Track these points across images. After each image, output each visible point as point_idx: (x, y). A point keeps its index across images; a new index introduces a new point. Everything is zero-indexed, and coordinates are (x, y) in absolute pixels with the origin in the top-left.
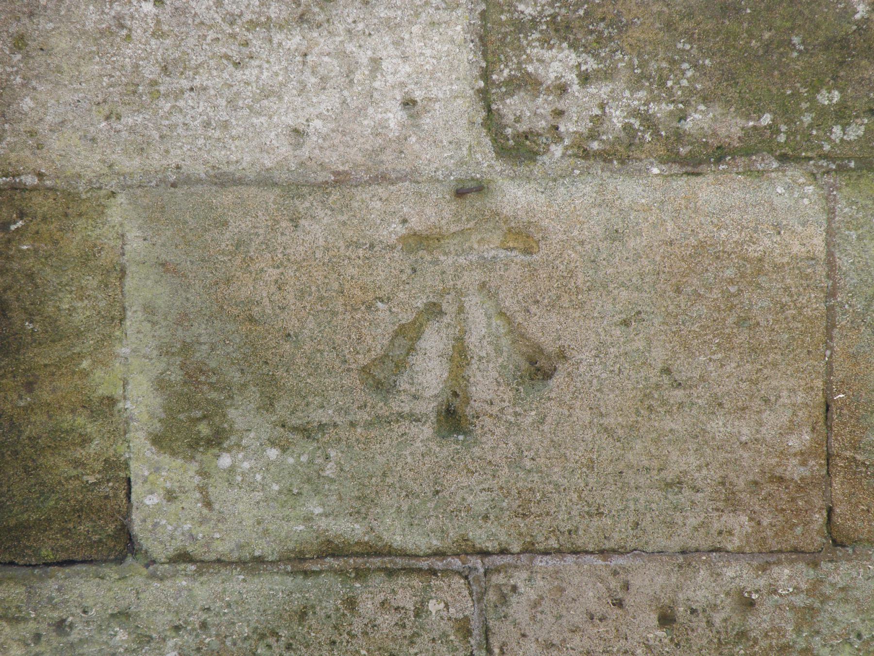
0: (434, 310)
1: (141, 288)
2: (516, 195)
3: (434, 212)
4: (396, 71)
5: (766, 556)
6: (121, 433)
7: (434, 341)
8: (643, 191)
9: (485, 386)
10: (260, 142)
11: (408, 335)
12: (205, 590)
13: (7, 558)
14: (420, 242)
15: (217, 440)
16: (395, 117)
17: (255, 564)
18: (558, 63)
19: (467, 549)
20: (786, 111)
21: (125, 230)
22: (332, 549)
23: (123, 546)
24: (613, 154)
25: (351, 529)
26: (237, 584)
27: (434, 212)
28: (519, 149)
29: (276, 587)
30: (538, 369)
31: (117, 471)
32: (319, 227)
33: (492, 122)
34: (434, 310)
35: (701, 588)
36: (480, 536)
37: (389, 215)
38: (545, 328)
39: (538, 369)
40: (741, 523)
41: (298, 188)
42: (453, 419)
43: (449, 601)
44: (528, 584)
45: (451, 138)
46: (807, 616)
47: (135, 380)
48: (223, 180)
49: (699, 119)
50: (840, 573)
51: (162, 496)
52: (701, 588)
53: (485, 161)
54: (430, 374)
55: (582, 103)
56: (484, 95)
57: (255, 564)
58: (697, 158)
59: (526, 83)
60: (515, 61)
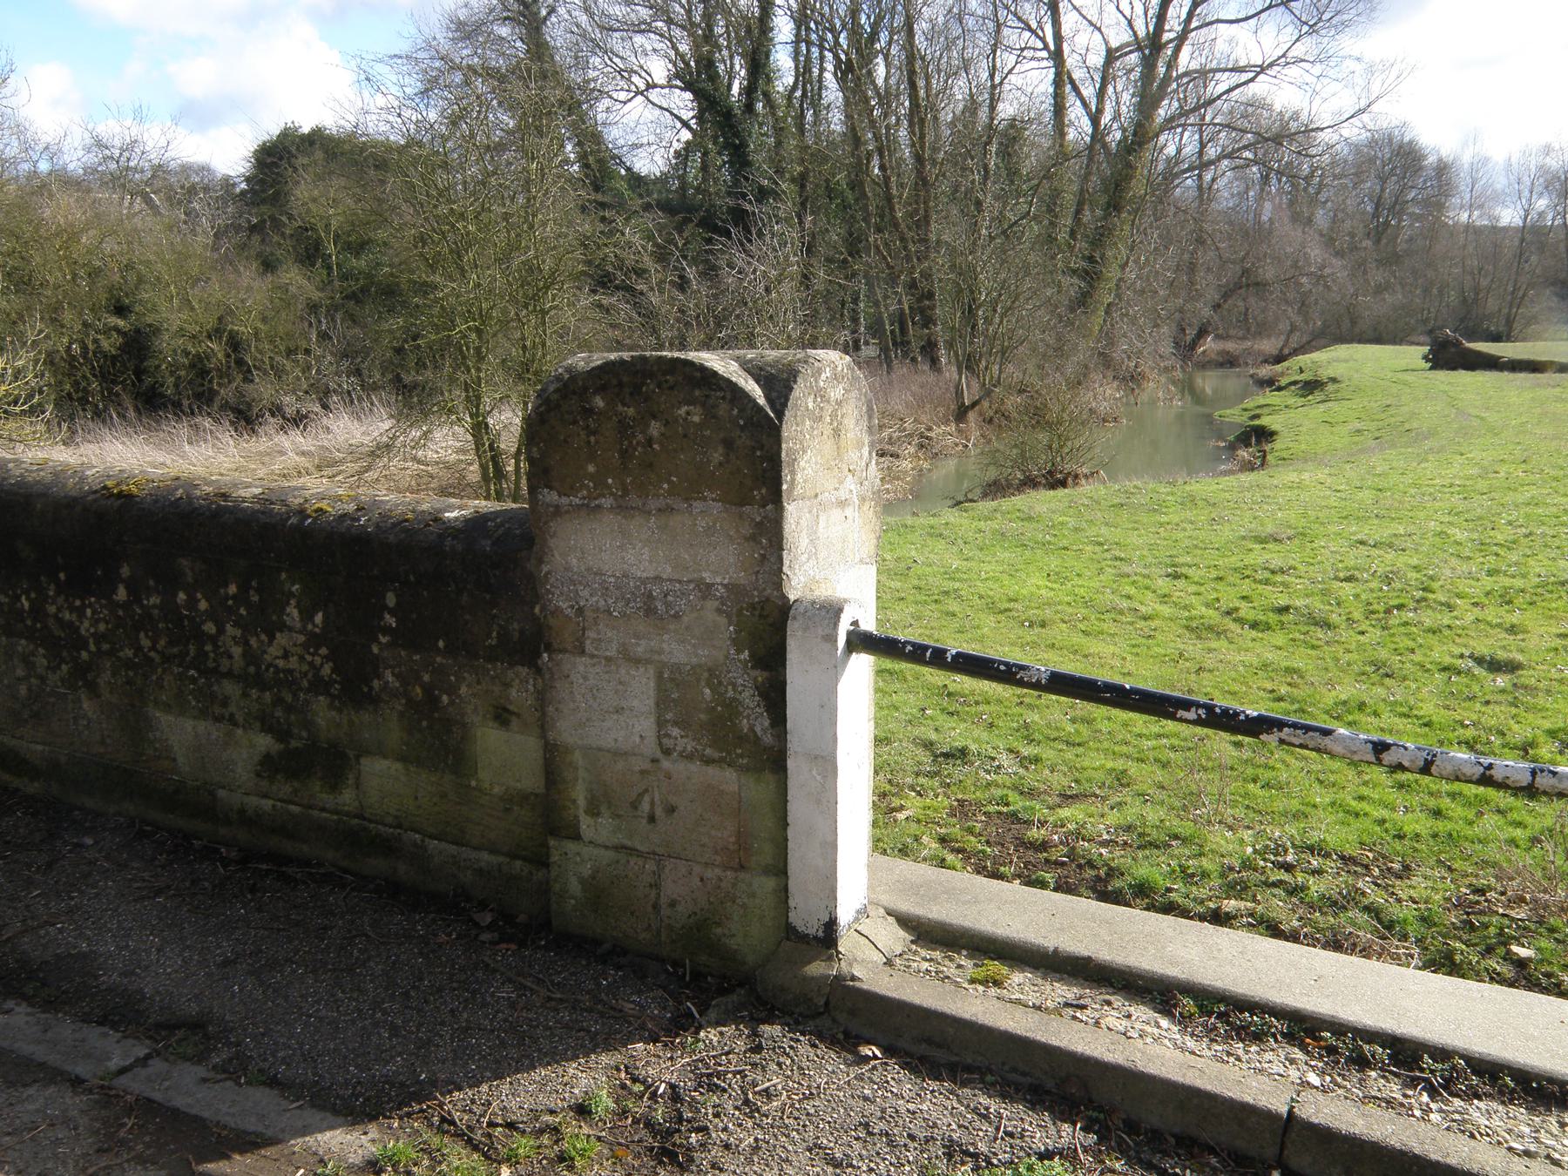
0: (646, 791)
1: (582, 773)
2: (666, 764)
3: (647, 766)
4: (638, 728)
5: (726, 868)
6: (577, 808)
7: (647, 798)
8: (695, 767)
9: (659, 812)
10: (608, 741)
11: (641, 795)
12: (596, 851)
13: (1545, 814)
14: (643, 772)
15: (598, 814)
16: (638, 740)
17: (606, 847)
18: (675, 732)
19: (654, 853)
20: (729, 753)
21: (577, 757)
22: (624, 847)
23: (577, 837)
24: (690, 757)
25: (629, 844)
26: (603, 851)
27: (647, 766)
28: (667, 752)
29: (611, 854)
30: (671, 810)
31: (576, 817)
32: (620, 765)
33: (660, 744)
34: (646, 791)
35: (709, 874)
36: (657, 850)
37: (639, 764)
38: (673, 800)
39: (671, 810)
40: (718, 858)
41: (618, 754)
42: (652, 819)
43: (650, 866)
44: (669, 864)
45: (650, 747)
46: (734, 885)
47: (580, 795)
48: (600, 749)
49: (708, 751)
50: (742, 875)
51: (586, 824)
52: (709, 874)
53: (659, 754)
54: (645, 806)
55: (681, 743)
56: (659, 737)
57: (606, 847)
58: (708, 761)
59: (668, 736)
60: (92, 648)
